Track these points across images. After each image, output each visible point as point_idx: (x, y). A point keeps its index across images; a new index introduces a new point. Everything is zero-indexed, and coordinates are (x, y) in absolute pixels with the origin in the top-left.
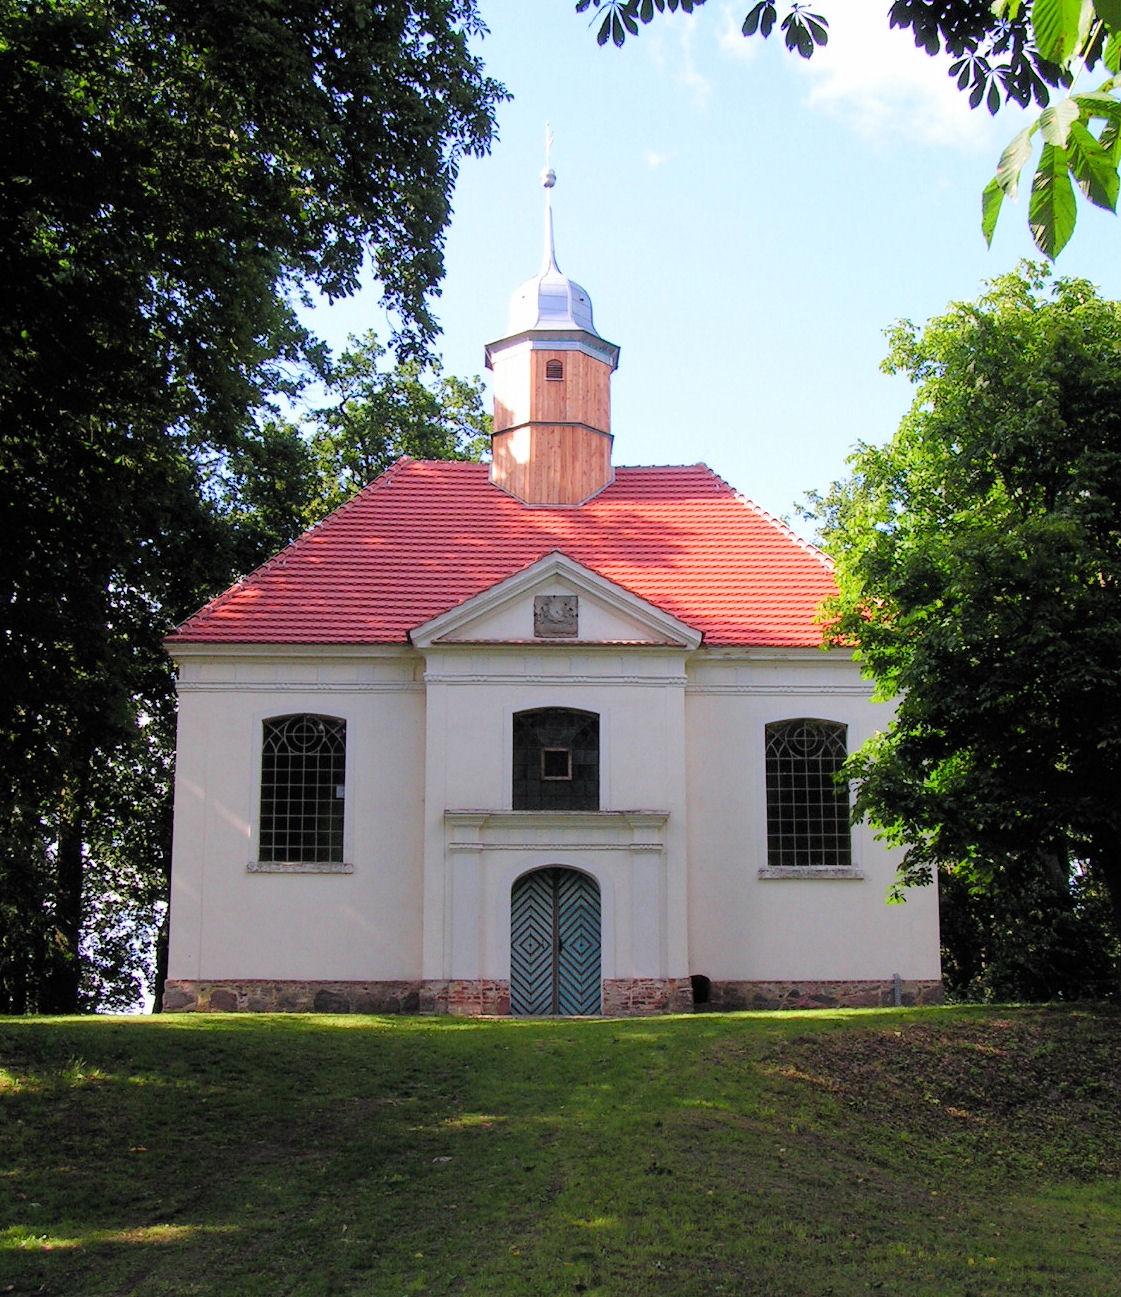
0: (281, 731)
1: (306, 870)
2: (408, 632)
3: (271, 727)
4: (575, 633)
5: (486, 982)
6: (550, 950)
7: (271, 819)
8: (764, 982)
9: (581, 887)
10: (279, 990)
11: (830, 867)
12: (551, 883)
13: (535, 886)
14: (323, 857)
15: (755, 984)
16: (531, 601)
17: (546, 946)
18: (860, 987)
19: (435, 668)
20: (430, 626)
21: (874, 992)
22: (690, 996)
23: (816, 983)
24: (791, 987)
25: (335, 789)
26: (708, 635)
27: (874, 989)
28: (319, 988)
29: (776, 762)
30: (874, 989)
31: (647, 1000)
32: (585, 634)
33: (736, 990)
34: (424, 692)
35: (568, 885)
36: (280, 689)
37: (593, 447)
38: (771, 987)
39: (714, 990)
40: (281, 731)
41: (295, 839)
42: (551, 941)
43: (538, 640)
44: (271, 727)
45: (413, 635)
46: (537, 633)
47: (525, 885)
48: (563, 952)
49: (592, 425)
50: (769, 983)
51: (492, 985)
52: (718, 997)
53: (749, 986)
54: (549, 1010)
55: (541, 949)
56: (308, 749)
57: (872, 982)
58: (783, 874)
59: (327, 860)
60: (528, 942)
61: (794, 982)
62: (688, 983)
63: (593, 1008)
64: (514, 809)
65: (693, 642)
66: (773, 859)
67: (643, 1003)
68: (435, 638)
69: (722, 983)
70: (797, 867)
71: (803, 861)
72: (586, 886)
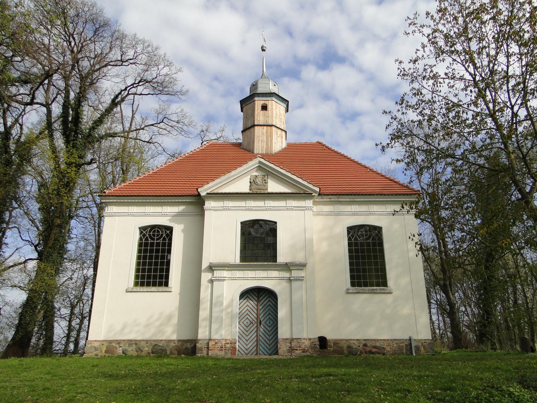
0: (146, 232)
1: (152, 290)
2: (197, 189)
3: (143, 230)
4: (267, 189)
5: (226, 340)
6: (255, 325)
7: (140, 268)
8: (351, 340)
9: (269, 296)
10: (136, 344)
11: (378, 288)
12: (256, 295)
13: (249, 296)
14: (160, 285)
15: (347, 340)
16: (249, 177)
17: (254, 323)
18: (395, 342)
19: (209, 204)
20: (206, 187)
21: (401, 345)
22: (318, 346)
23: (375, 340)
24: (364, 342)
25: (167, 256)
26: (322, 189)
27: (401, 343)
28: (154, 343)
29: (352, 243)
30: (401, 343)
31: (298, 349)
32: (270, 190)
33: (339, 343)
34: (203, 215)
35: (264, 295)
36: (146, 215)
37: (279, 134)
38: (354, 342)
39: (329, 343)
40: (146, 232)
41: (149, 277)
42: (256, 320)
43: (251, 192)
44: (143, 230)
45: (199, 190)
46: (250, 189)
47: (246, 294)
48: (262, 326)
49: (278, 126)
50: (353, 340)
51: (229, 342)
52: (330, 347)
53: (345, 342)
54: (255, 353)
55: (252, 325)
56: (157, 240)
57: (400, 340)
58: (357, 291)
59: (150, 286)
60: (246, 322)
61: (365, 340)
62: (317, 340)
63: (274, 352)
64: (240, 262)
65: (315, 191)
66: (353, 284)
67: (297, 350)
68: (209, 191)
69: (332, 340)
70: (363, 288)
71: (365, 285)
72: (272, 297)
